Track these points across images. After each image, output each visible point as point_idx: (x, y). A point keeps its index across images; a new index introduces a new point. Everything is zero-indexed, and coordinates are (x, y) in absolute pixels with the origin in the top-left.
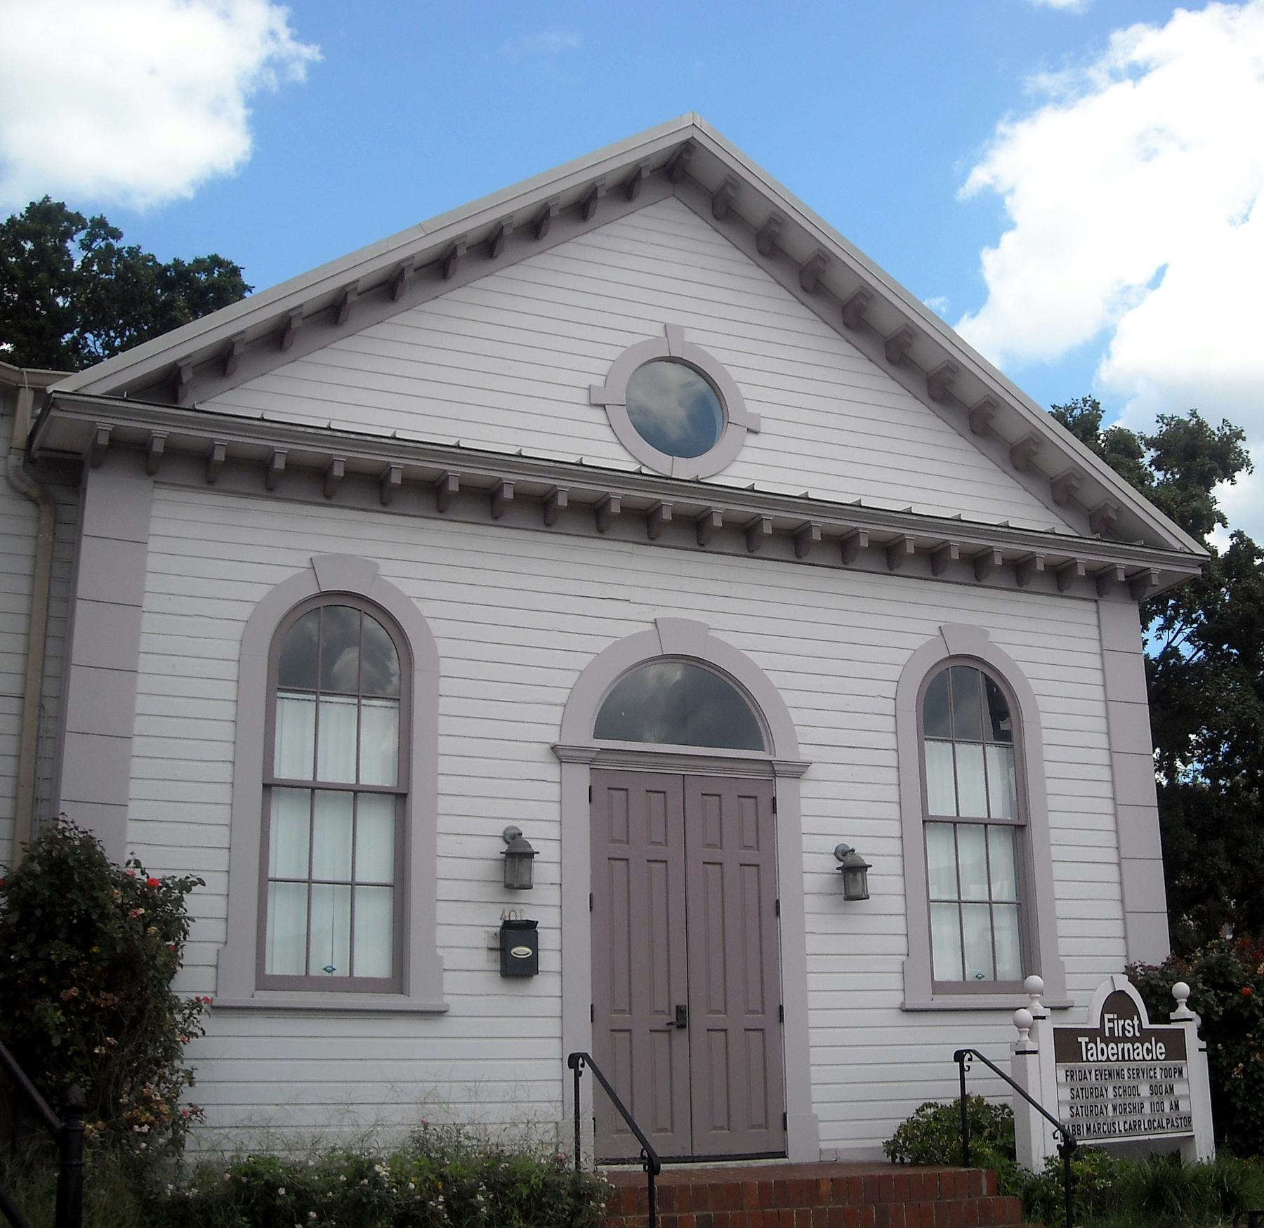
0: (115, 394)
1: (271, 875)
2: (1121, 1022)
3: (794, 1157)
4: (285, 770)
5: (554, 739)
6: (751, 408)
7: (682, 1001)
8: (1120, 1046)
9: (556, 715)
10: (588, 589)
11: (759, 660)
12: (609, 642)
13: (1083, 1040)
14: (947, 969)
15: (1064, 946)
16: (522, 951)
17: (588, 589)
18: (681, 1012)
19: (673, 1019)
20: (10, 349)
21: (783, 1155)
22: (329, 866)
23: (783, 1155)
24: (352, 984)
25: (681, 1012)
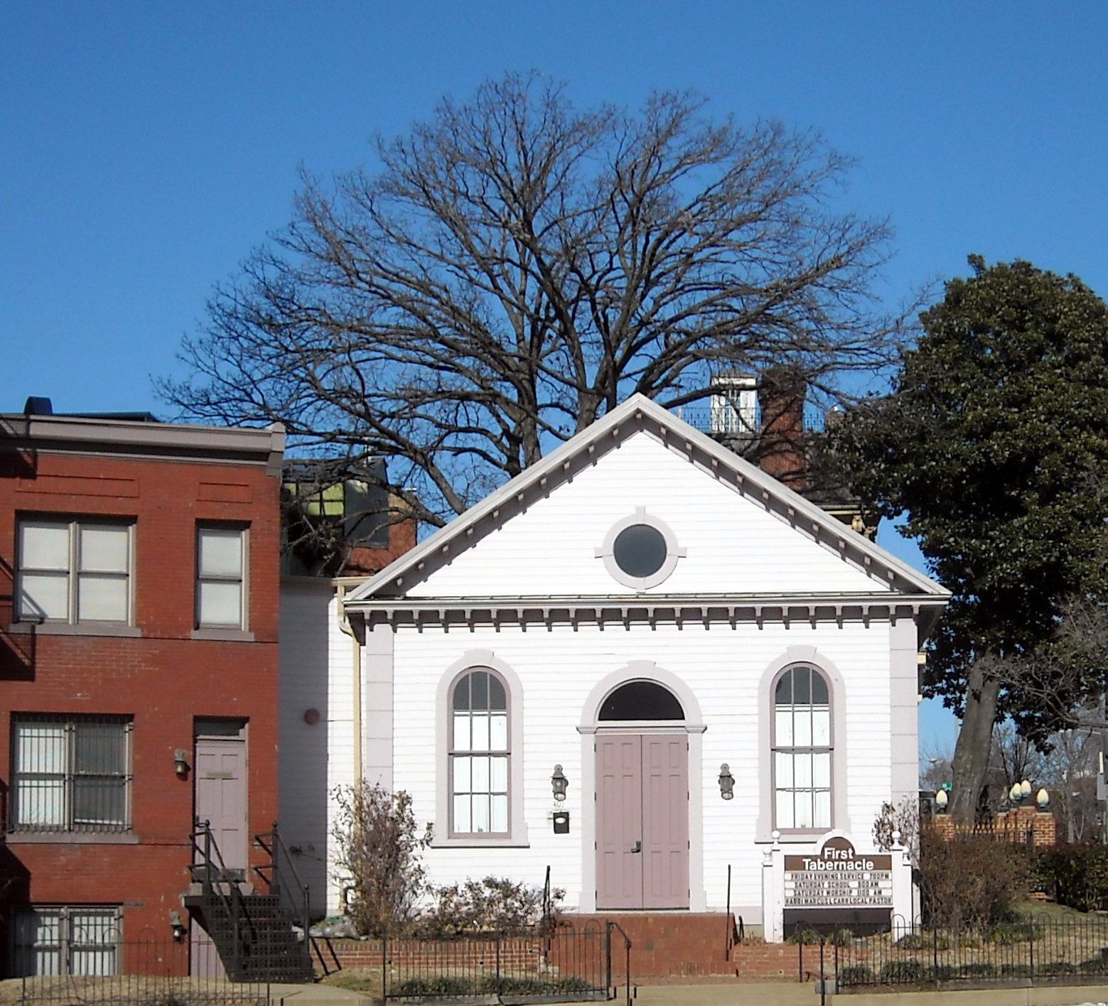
0: (368, 598)
1: (456, 790)
2: (838, 852)
3: (692, 910)
4: (458, 748)
5: (578, 723)
6: (681, 544)
7: (640, 840)
8: (836, 863)
9: (580, 712)
10: (56, 805)
11: (682, 676)
12: (604, 675)
13: (807, 861)
14: (784, 821)
15: (851, 810)
16: (560, 821)
17: (56, 805)
18: (639, 844)
19: (635, 847)
20: (925, 334)
21: (688, 909)
22: (480, 785)
23: (688, 909)
24: (491, 835)
25: (639, 844)
